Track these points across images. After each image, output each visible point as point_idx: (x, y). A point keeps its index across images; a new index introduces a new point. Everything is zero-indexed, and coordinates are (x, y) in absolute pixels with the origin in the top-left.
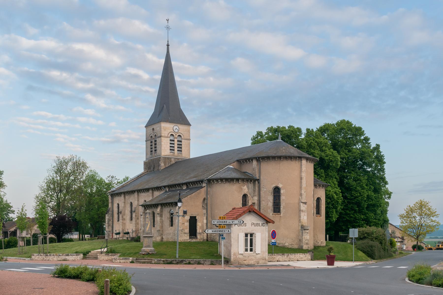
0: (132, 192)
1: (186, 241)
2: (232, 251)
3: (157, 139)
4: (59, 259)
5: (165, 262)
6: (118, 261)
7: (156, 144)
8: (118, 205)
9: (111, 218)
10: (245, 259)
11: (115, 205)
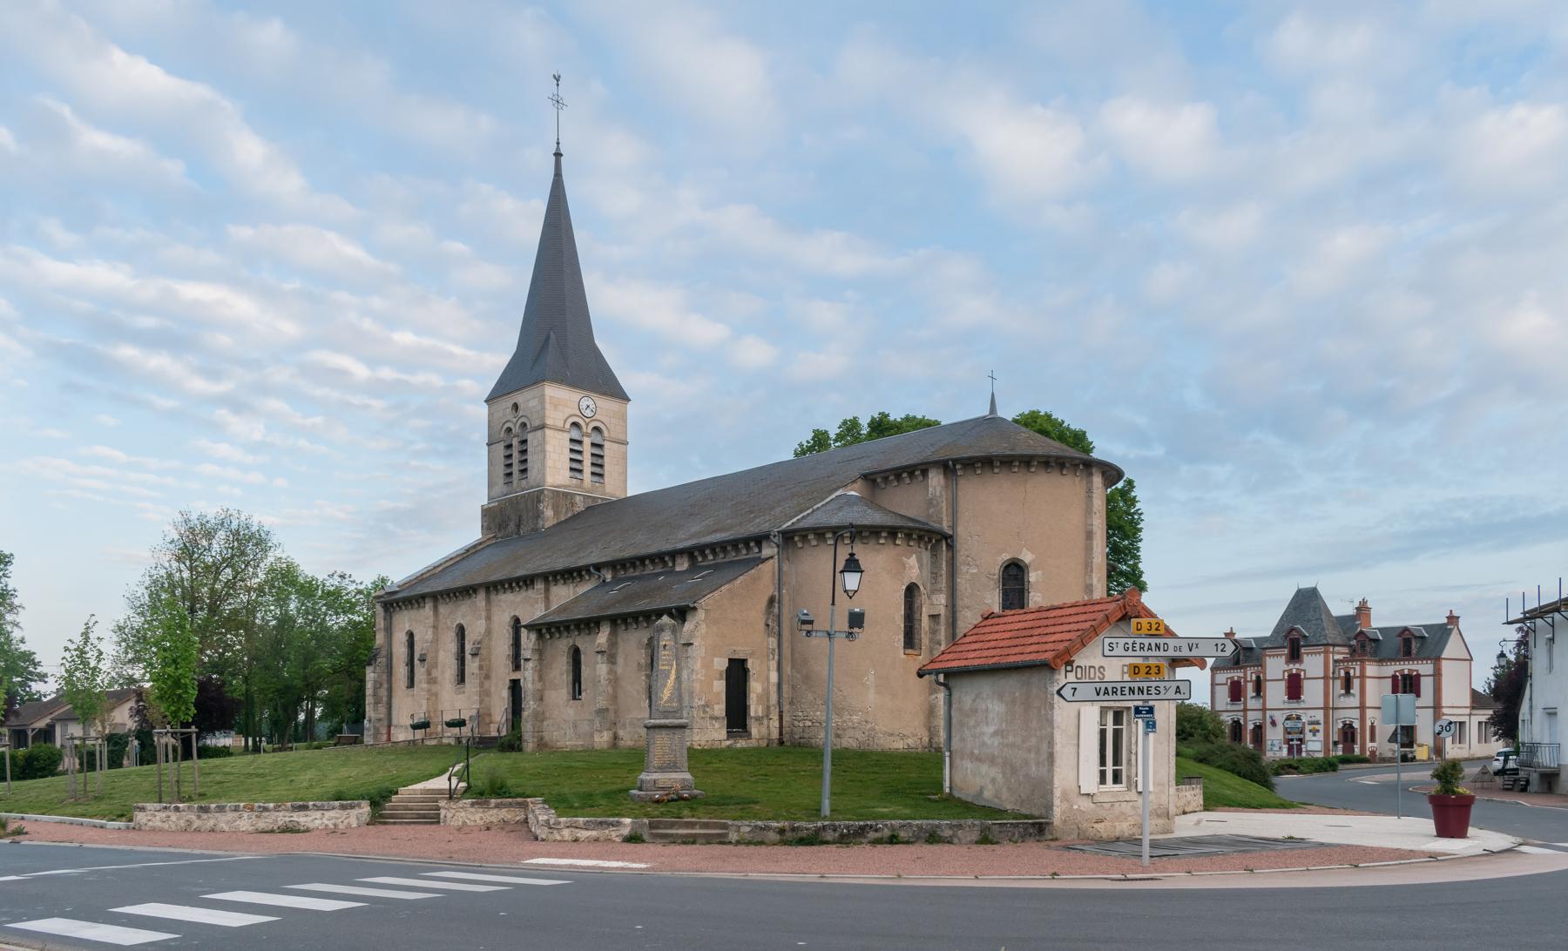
0: (468, 591)
1: (716, 745)
2: (1056, 782)
3: (530, 437)
4: (261, 825)
5: (789, 835)
6: (566, 832)
7: (524, 452)
8: (411, 635)
9: (385, 677)
10: (1102, 813)
11: (400, 639)
